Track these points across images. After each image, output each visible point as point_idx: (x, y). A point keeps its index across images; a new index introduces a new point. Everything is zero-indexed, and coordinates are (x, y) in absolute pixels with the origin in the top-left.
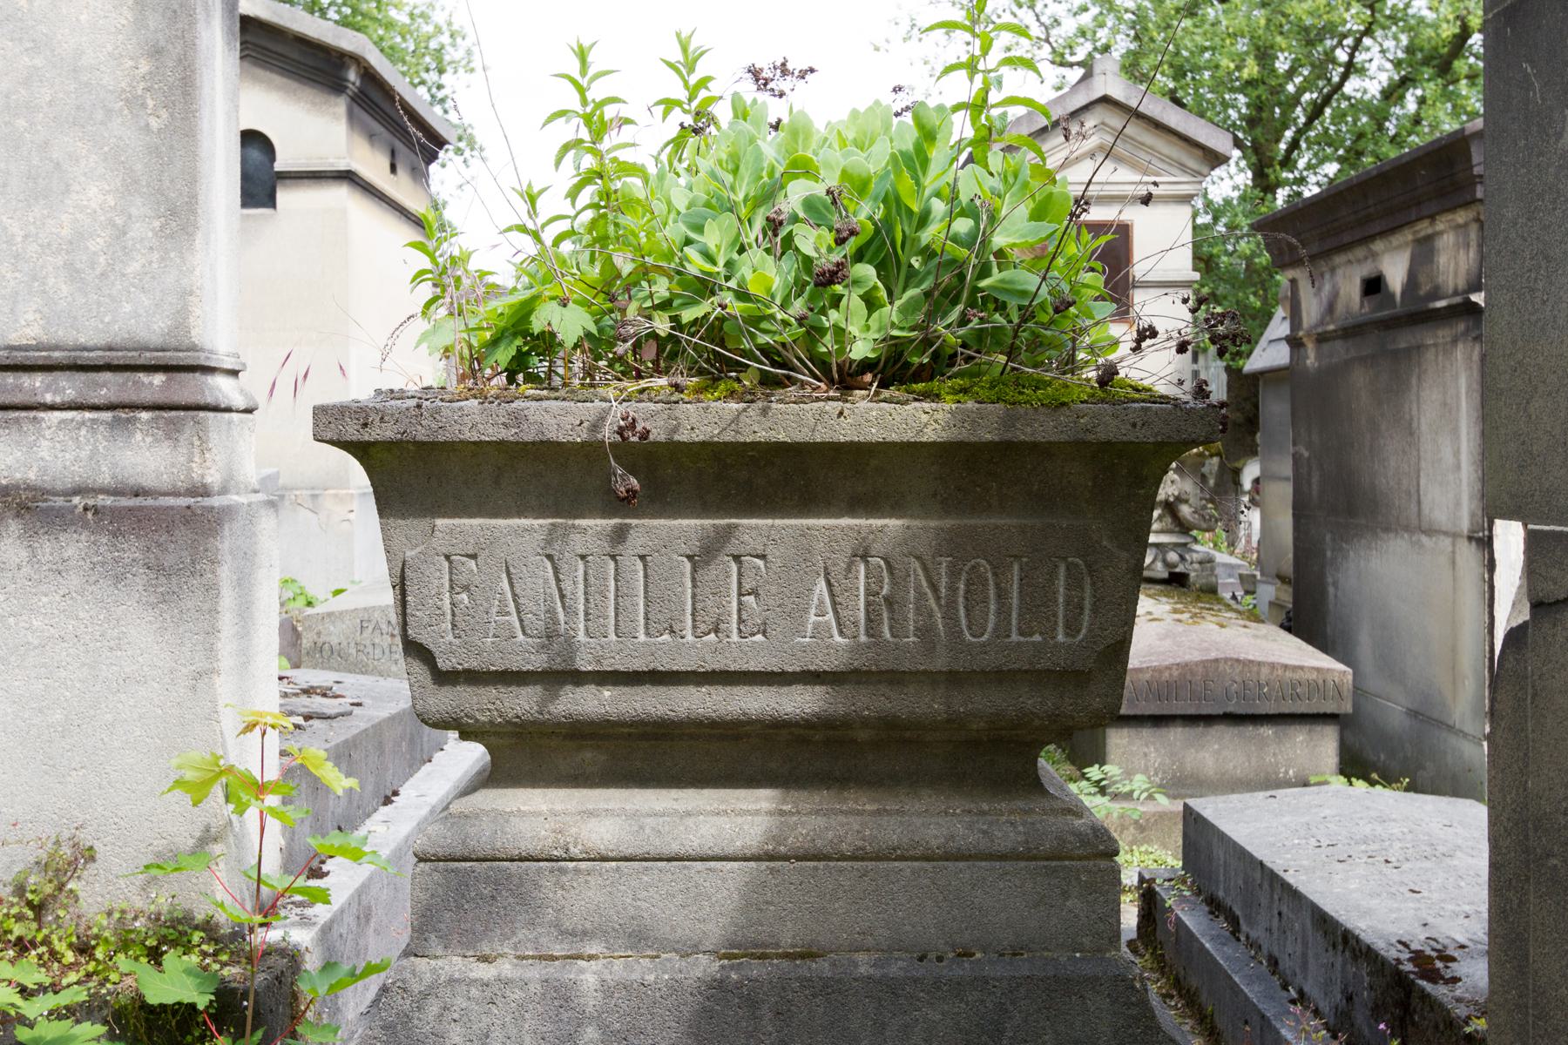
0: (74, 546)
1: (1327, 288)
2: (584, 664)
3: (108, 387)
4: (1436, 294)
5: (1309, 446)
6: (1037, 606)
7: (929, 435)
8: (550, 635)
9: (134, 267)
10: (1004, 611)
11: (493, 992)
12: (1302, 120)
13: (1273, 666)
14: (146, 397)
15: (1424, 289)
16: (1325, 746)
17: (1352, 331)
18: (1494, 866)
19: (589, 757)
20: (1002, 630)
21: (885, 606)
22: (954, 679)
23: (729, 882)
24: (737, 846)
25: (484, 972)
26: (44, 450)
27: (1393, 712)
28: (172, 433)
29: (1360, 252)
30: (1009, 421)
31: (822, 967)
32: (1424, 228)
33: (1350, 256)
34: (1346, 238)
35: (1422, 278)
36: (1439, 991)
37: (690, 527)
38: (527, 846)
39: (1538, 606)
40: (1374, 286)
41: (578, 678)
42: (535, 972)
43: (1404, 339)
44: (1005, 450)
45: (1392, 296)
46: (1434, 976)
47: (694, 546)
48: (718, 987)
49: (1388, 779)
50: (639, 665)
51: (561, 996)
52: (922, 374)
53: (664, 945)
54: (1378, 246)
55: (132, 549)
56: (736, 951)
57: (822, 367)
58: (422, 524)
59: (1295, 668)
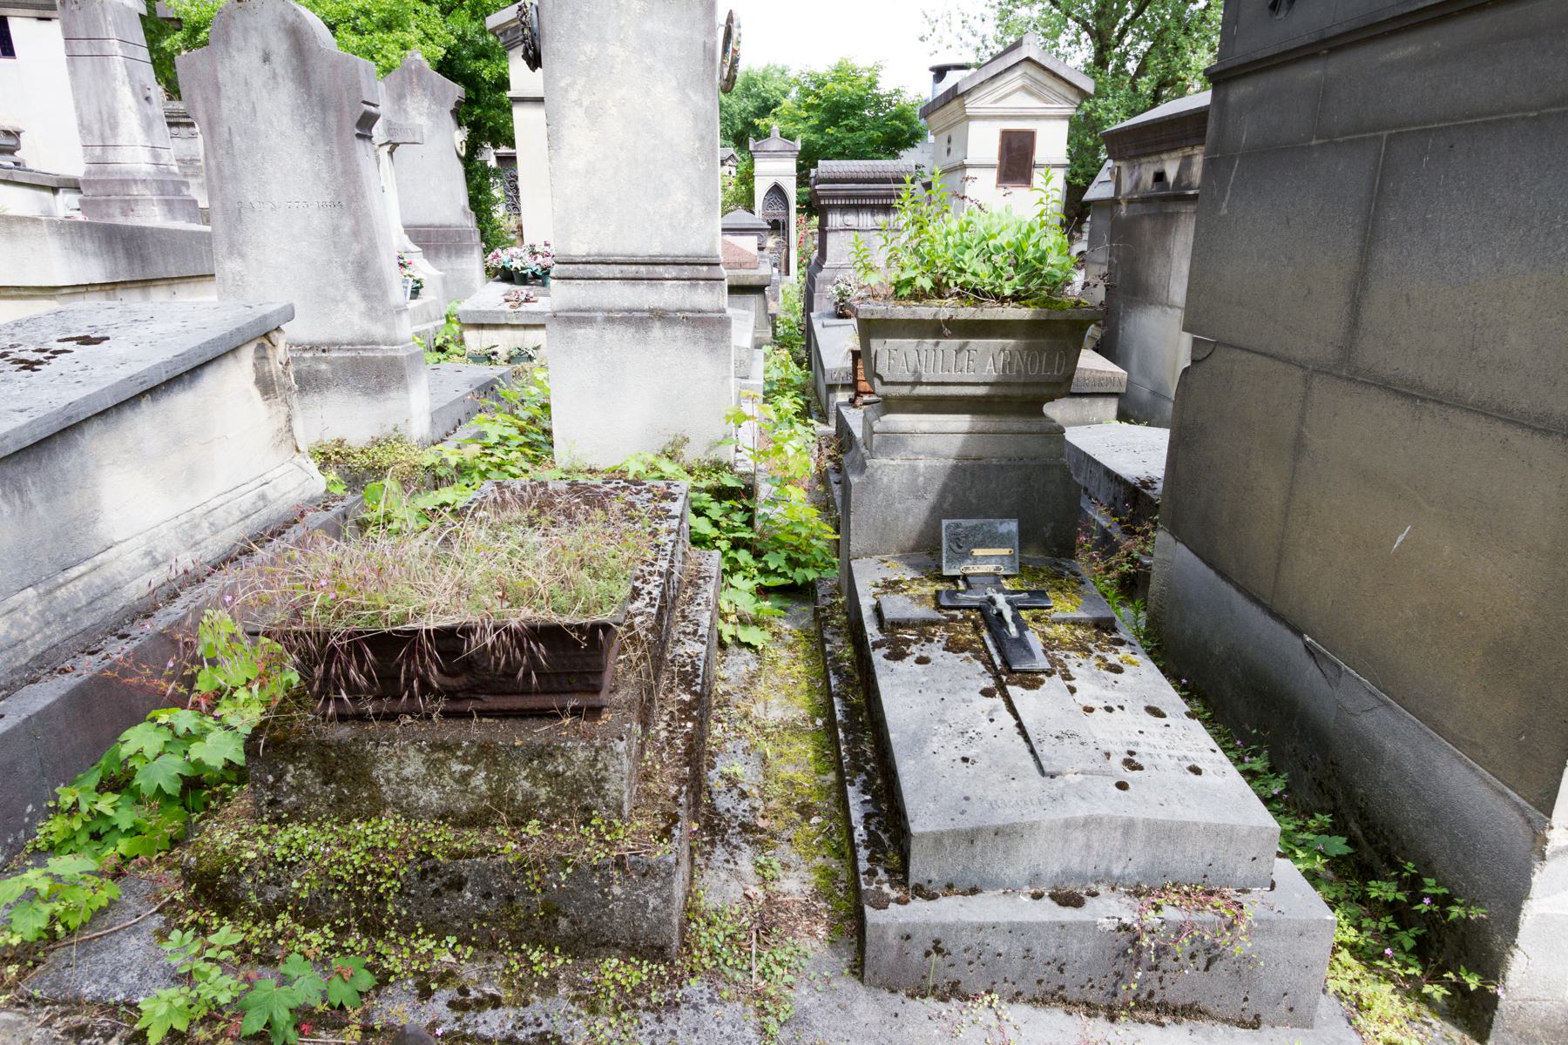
0: (679, 331)
1: (1136, 174)
2: (924, 380)
3: (687, 271)
4: (1189, 187)
5: (1118, 257)
6: (1050, 364)
7: (1027, 318)
8: (915, 372)
9: (695, 225)
10: (1040, 366)
11: (895, 468)
12: (1132, 11)
13: (1091, 371)
14: (702, 276)
15: (1184, 183)
16: (1112, 406)
17: (1146, 200)
18: (1170, 442)
19: (918, 405)
20: (1040, 371)
21: (1008, 365)
22: (1025, 384)
23: (958, 441)
24: (962, 430)
25: (892, 462)
26: (666, 295)
27: (1144, 393)
28: (712, 288)
29: (1155, 158)
30: (1048, 314)
31: (983, 462)
32: (1188, 151)
33: (1150, 159)
34: (1149, 150)
35: (1184, 177)
36: (1149, 492)
37: (957, 342)
38: (905, 430)
39: (1193, 361)
40: (1160, 177)
41: (921, 384)
42: (907, 463)
43: (1171, 208)
44: (1047, 322)
45: (1168, 184)
46: (1148, 488)
47: (957, 347)
48: (955, 467)
49: (1138, 422)
50: (939, 380)
51: (914, 469)
52: (1024, 299)
53: (941, 456)
54: (1164, 156)
55: (700, 333)
56: (960, 458)
57: (997, 297)
58: (882, 341)
59: (1102, 372)
